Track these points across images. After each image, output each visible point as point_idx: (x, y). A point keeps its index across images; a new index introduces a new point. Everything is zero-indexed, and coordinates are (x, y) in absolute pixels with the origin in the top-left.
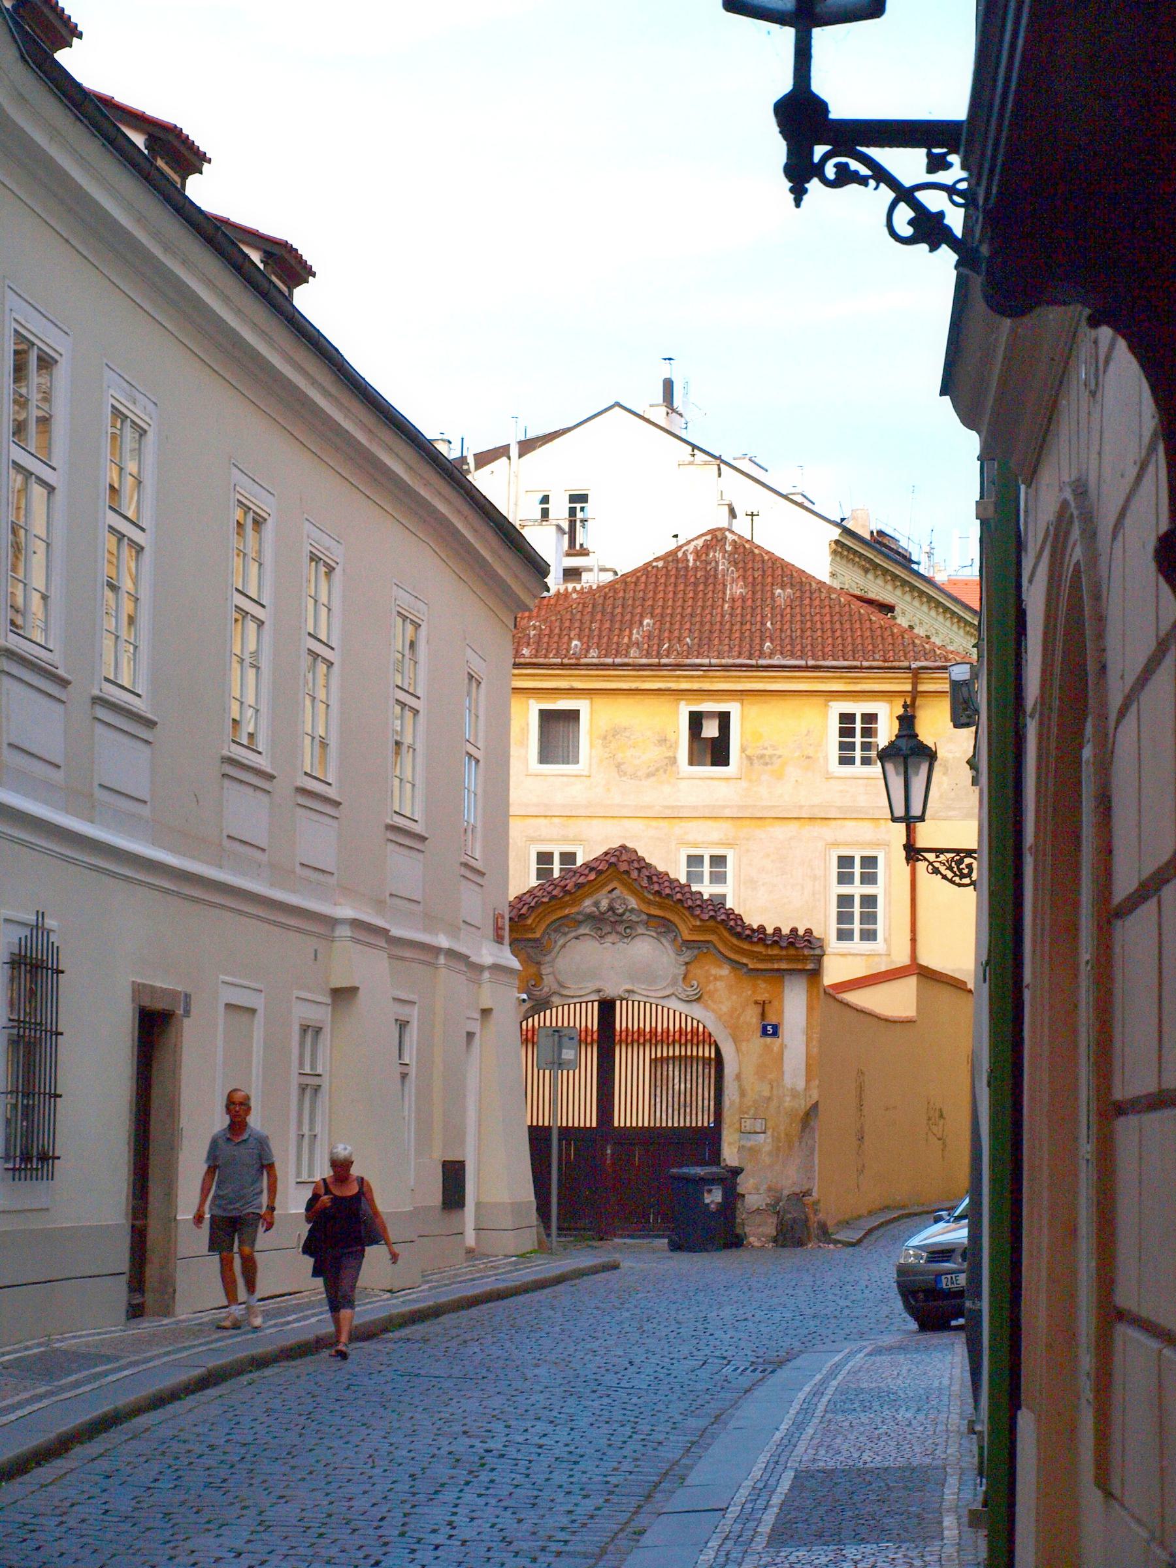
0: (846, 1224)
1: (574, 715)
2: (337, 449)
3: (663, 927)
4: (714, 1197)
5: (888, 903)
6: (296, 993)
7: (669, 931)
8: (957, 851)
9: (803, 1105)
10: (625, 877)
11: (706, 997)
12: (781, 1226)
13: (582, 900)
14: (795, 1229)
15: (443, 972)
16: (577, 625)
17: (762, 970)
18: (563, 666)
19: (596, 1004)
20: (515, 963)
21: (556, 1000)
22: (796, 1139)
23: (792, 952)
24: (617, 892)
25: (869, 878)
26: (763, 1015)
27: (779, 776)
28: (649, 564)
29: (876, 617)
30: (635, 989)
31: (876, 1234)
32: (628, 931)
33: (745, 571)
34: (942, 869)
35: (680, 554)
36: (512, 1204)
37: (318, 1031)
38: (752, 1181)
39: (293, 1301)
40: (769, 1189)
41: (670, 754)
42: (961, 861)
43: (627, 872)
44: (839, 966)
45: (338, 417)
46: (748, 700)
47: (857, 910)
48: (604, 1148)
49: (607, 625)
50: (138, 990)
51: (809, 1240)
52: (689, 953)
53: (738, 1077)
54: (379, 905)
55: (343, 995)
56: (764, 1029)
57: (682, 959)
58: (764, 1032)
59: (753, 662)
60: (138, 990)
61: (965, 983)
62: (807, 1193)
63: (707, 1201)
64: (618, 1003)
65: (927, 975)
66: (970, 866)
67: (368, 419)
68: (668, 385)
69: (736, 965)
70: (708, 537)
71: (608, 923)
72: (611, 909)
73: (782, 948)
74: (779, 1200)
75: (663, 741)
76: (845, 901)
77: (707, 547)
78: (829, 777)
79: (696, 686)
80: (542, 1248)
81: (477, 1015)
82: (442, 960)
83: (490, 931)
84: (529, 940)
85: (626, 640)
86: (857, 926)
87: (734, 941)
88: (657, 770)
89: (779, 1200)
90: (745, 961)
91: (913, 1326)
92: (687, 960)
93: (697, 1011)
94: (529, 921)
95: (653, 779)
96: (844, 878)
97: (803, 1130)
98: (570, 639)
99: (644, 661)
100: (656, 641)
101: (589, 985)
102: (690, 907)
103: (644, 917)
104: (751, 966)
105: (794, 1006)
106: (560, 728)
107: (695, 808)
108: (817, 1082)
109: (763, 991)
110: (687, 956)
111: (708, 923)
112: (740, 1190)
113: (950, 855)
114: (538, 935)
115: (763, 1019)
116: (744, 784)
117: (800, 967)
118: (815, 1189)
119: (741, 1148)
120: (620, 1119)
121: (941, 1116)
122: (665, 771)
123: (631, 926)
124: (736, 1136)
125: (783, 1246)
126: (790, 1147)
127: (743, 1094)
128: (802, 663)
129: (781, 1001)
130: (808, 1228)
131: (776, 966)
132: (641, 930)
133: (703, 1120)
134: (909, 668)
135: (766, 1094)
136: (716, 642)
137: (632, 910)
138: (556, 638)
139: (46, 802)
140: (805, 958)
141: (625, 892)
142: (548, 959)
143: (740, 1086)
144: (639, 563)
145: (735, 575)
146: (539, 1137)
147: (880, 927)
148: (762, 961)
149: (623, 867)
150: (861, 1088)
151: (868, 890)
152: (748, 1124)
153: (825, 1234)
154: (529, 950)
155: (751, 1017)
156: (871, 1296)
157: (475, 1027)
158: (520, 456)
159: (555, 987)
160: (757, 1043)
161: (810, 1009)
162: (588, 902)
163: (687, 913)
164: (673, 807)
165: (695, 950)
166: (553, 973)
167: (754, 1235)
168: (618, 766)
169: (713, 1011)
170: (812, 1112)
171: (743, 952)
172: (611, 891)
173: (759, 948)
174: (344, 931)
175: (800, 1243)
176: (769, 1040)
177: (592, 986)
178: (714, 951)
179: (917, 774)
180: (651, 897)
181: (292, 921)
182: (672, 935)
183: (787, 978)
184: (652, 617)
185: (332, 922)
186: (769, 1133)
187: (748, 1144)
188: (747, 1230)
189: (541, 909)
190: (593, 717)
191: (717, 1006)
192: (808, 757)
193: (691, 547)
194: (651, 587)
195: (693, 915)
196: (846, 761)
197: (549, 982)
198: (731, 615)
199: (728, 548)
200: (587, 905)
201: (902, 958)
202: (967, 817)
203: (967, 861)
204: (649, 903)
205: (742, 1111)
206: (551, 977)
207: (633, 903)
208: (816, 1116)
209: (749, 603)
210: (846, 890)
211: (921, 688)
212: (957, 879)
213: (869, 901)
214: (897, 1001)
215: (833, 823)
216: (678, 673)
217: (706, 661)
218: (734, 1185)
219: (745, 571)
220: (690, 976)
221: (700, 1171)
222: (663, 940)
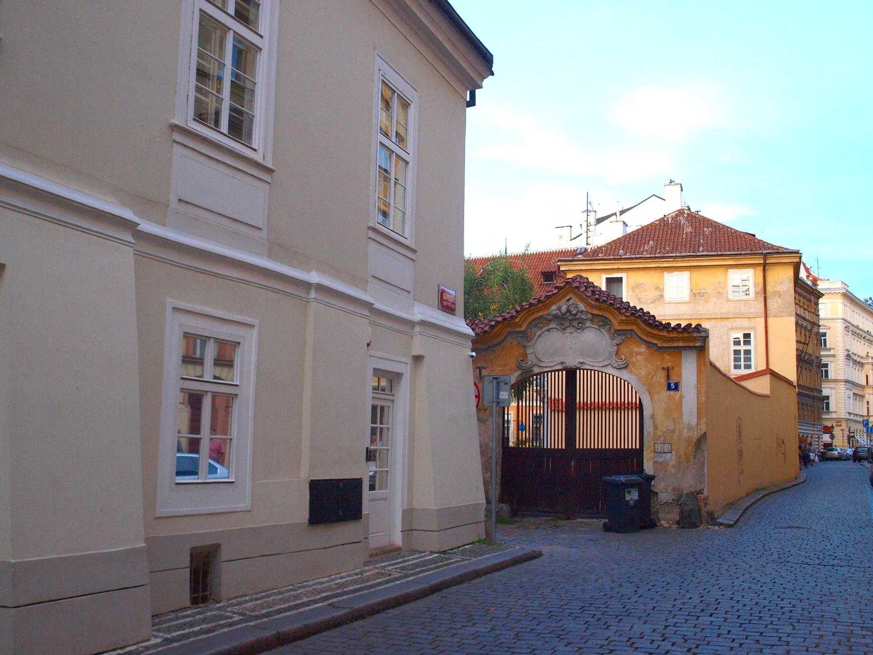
1: (620, 280)
3: (603, 322)
4: (633, 496)
5: (756, 353)
7: (605, 324)
9: (695, 435)
11: (630, 366)
13: (550, 306)
15: (313, 305)
17: (666, 348)
18: (615, 259)
20: (469, 331)
24: (571, 301)
31: (749, 512)
36: (440, 511)
40: (674, 489)
43: (577, 287)
47: (742, 356)
51: (701, 523)
52: (619, 338)
53: (652, 417)
56: (669, 384)
57: (615, 342)
62: (700, 492)
65: (774, 375)
69: (647, 343)
71: (569, 321)
72: (569, 311)
74: (681, 496)
75: (657, 288)
76: (737, 352)
77: (677, 216)
79: (670, 265)
81: (409, 360)
82: (313, 295)
86: (742, 363)
87: (648, 329)
90: (655, 342)
93: (625, 375)
94: (517, 320)
97: (696, 451)
101: (557, 359)
103: (590, 316)
105: (688, 370)
110: (618, 339)
114: (523, 329)
118: (705, 489)
119: (655, 463)
123: (582, 322)
124: (652, 455)
126: (688, 461)
127: (656, 427)
129: (680, 367)
130: (701, 516)
131: (675, 345)
135: (671, 427)
137: (582, 312)
140: (695, 339)
143: (654, 423)
148: (666, 341)
151: (747, 348)
153: (712, 519)
159: (535, 361)
160: (665, 394)
161: (699, 372)
162: (554, 307)
165: (622, 336)
166: (534, 353)
168: (639, 299)
169: (636, 374)
170: (701, 441)
171: (654, 336)
172: (568, 300)
173: (664, 333)
175: (695, 526)
176: (672, 393)
182: (608, 327)
183: (683, 352)
186: (674, 453)
187: (660, 460)
188: (660, 515)
195: (620, 313)
197: (531, 359)
201: (764, 367)
204: (592, 306)
207: (582, 307)
208: (705, 442)
211: (768, 262)
213: (747, 352)
214: (761, 386)
220: (620, 353)
221: (622, 478)
222: (603, 331)
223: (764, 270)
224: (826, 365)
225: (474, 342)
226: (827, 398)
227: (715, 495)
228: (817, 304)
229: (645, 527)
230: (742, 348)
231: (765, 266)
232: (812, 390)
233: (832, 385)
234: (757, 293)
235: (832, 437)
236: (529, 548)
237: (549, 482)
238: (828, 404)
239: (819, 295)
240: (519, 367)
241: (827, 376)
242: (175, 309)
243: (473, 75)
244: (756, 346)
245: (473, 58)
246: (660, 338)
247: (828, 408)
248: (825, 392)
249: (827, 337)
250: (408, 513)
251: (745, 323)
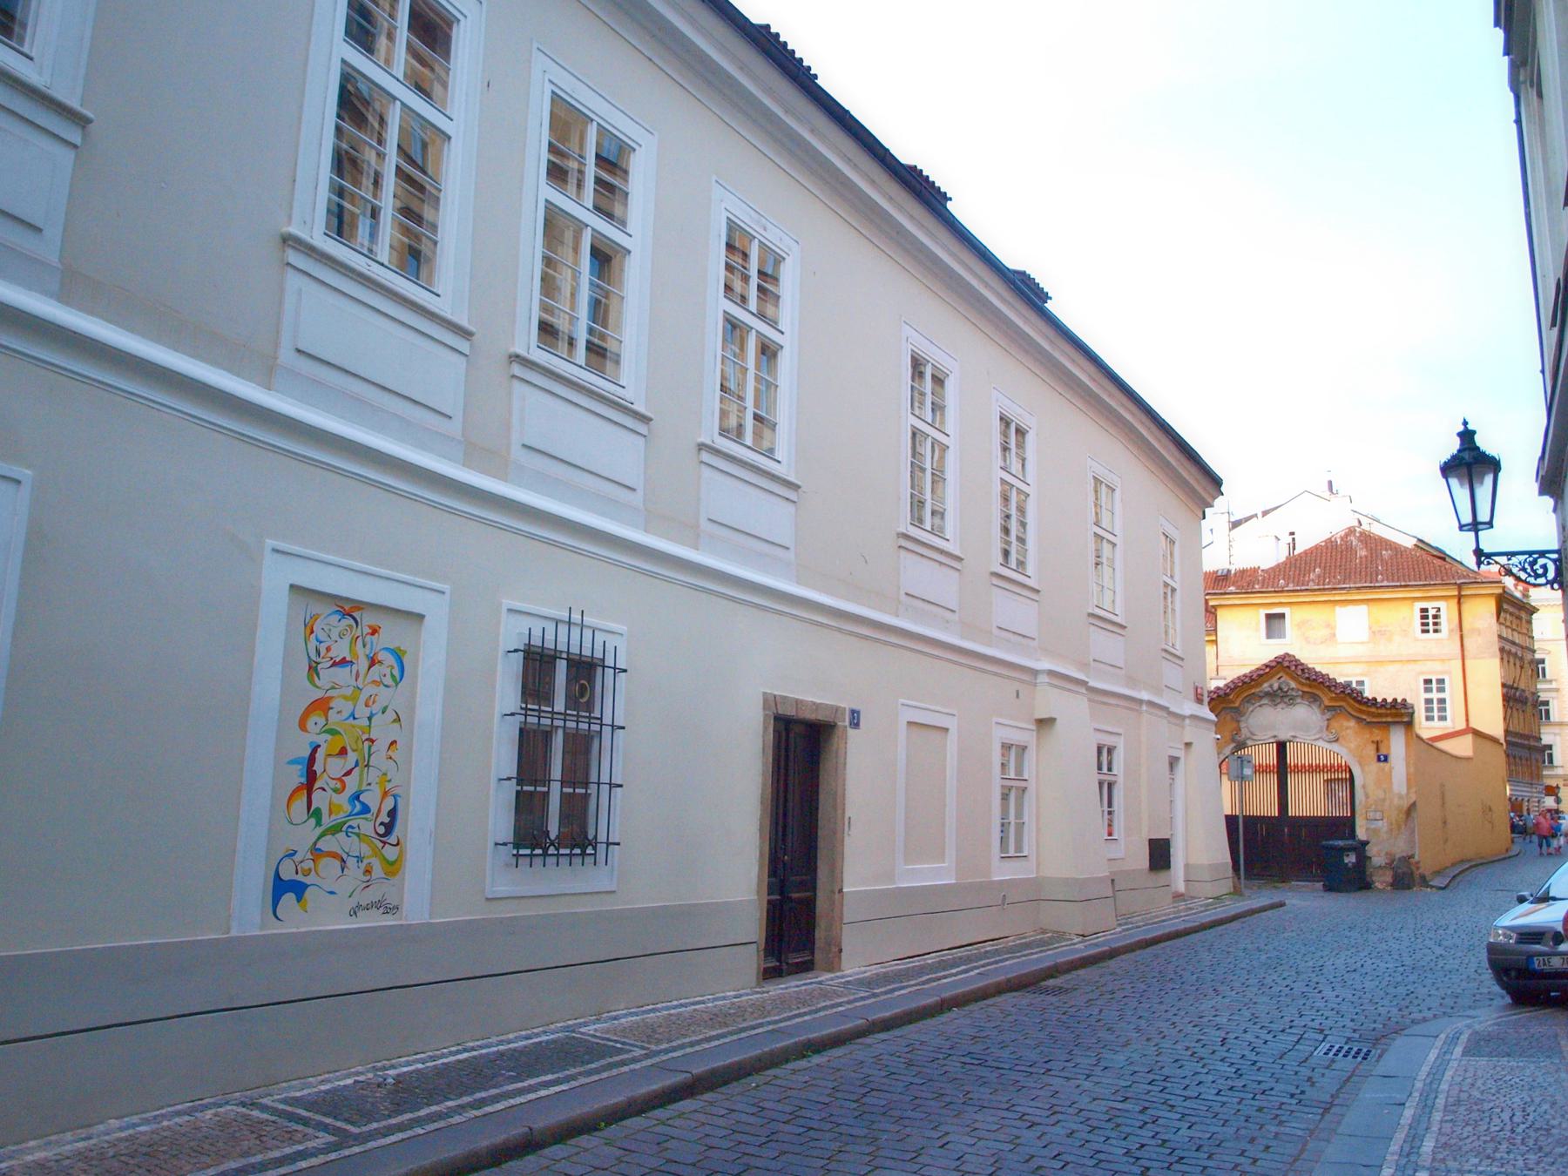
0: (1438, 873)
1: (1282, 616)
2: (1026, 352)
3: (1313, 698)
4: (1351, 859)
6: (995, 719)
8: (1530, 553)
9: (1406, 804)
14: (1405, 878)
20: (1212, 717)
21: (1249, 743)
25: (1441, 690)
29: (1438, 562)
34: (1515, 570)
37: (1024, 748)
39: (1000, 945)
42: (1535, 562)
44: (1426, 728)
45: (1020, 323)
50: (770, 701)
53: (1364, 787)
54: (1083, 666)
55: (1044, 723)
58: (1379, 760)
60: (770, 701)
62: (1412, 856)
65: (1477, 734)
66: (1544, 567)
67: (1050, 332)
68: (1330, 483)
69: (1359, 720)
71: (1279, 697)
75: (1328, 626)
77: (1347, 535)
78: (1416, 640)
80: (1236, 892)
82: (1144, 707)
83: (1192, 696)
91: (1508, 1000)
93: (1335, 747)
96: (1428, 690)
105: (1397, 743)
106: (1276, 622)
109: (1377, 734)
110: (1328, 715)
113: (1522, 558)
123: (1292, 698)
126: (1399, 827)
127: (1367, 796)
139: (443, 456)
146: (1231, 821)
147: (1448, 714)
151: (1441, 695)
153: (1424, 882)
156: (1458, 942)
157: (1180, 753)
160: (1375, 766)
161: (1407, 745)
170: (1410, 810)
174: (1043, 679)
179: (1482, 483)
181: (988, 667)
185: (1035, 673)
190: (1293, 616)
191: (1346, 746)
196: (1424, 631)
197: (1244, 732)
201: (1461, 725)
203: (1541, 561)
207: (1293, 685)
210: (1428, 696)
212: (1532, 580)
213: (1442, 701)
214: (1463, 747)
221: (1341, 843)
223: (1459, 603)
224: (1546, 703)
225: (1216, 724)
226: (1550, 747)
227: (1426, 860)
228: (1530, 622)
229: (1360, 889)
230: (1435, 695)
231: (1460, 598)
232: (1527, 737)
233: (1556, 730)
234: (1451, 631)
235: (1558, 801)
236: (1276, 900)
237: (1276, 849)
238: (1551, 756)
239: (1532, 610)
240: (1233, 740)
241: (1548, 717)
242: (510, 610)
243: (1206, 496)
244: (1453, 694)
245: (1204, 482)
246: (1369, 714)
247: (1551, 761)
248: (1546, 740)
249: (1547, 665)
250: (1187, 866)
251: (1437, 666)
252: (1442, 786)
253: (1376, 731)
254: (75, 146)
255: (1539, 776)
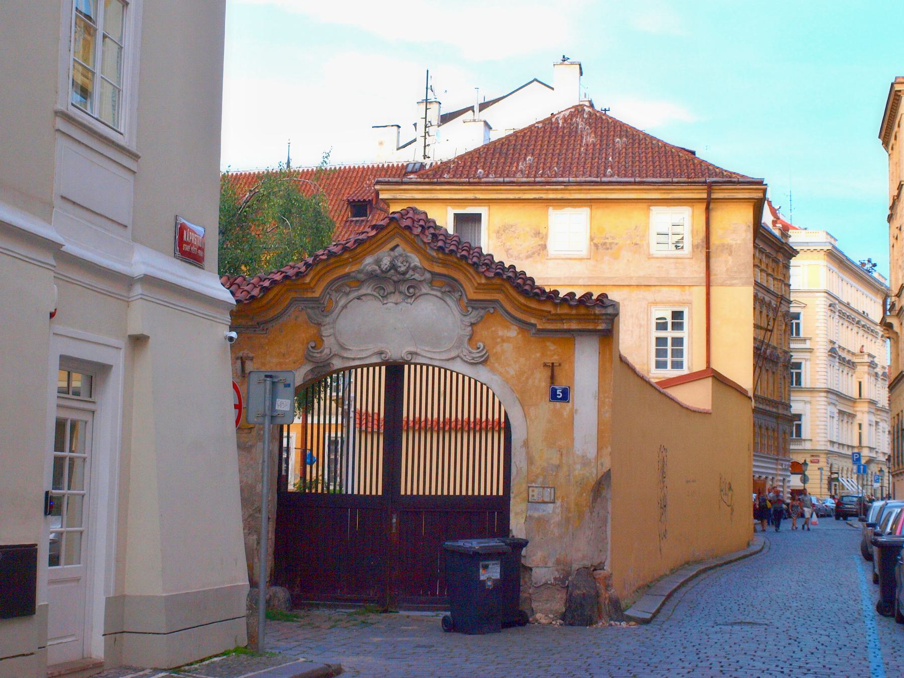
1: (477, 218)
4: (491, 573)
5: (691, 344)
7: (453, 290)
9: (593, 474)
10: (407, 233)
11: (492, 360)
12: (569, 601)
13: (364, 257)
14: (585, 605)
16: (482, 160)
18: (470, 183)
19: (383, 368)
22: (587, 510)
23: (583, 311)
24: (399, 250)
25: (678, 326)
26: (552, 377)
27: (616, 257)
28: (533, 125)
30: (419, 351)
32: (411, 290)
33: (596, 129)
35: (554, 120)
36: (168, 599)
38: (539, 554)
40: (558, 562)
41: (542, 243)
43: (408, 228)
44: (636, 340)
46: (594, 206)
47: (669, 347)
48: (391, 519)
49: (502, 160)
51: (600, 617)
52: (475, 313)
53: (526, 444)
58: (554, 397)
59: (599, 179)
61: (747, 392)
62: (599, 567)
63: (482, 578)
64: (406, 367)
65: (720, 380)
69: (524, 326)
70: (573, 110)
71: (393, 283)
72: (393, 267)
73: (571, 306)
74: (567, 574)
75: (537, 234)
76: (661, 341)
77: (572, 115)
79: (559, 196)
81: (122, 343)
84: (306, 300)
85: (514, 169)
86: (669, 359)
87: (522, 300)
88: (533, 253)
89: (566, 577)
90: (533, 321)
92: (473, 321)
94: (308, 280)
95: (530, 259)
97: (594, 500)
98: (477, 169)
99: (525, 180)
100: (534, 169)
101: (371, 346)
102: (475, 263)
104: (539, 327)
105: (585, 369)
107: (559, 279)
108: (609, 449)
109: (553, 351)
110: (474, 316)
111: (494, 281)
112: (527, 562)
114: (317, 295)
115: (552, 383)
116: (592, 262)
117: (591, 327)
119: (528, 519)
120: (406, 488)
121: (730, 488)
122: (539, 254)
123: (414, 285)
125: (572, 625)
126: (581, 516)
127: (530, 461)
128: (632, 180)
129: (572, 363)
131: (566, 326)
132: (425, 289)
133: (492, 487)
134: (705, 182)
135: (555, 461)
136: (575, 169)
137: (415, 269)
138: (467, 168)
140: (596, 318)
141: (408, 249)
142: (328, 320)
143: (528, 453)
144: (526, 125)
145: (589, 131)
149: (406, 223)
150: (663, 464)
151: (677, 334)
152: (535, 493)
153: (617, 611)
154: (309, 311)
155: (540, 380)
158: (480, 111)
159: (336, 349)
160: (545, 408)
161: (602, 372)
162: (369, 260)
163: (471, 271)
164: (544, 279)
165: (480, 310)
167: (541, 612)
169: (501, 374)
172: (393, 249)
173: (548, 307)
176: (558, 405)
177: (373, 348)
178: (501, 311)
180: (434, 254)
182: (457, 295)
184: (533, 155)
186: (558, 503)
187: (536, 514)
188: (534, 605)
189: (319, 267)
191: (501, 375)
192: (636, 244)
193: (561, 116)
194: (534, 138)
195: (478, 272)
197: (329, 343)
198: (586, 154)
199: (586, 116)
200: (369, 261)
201: (701, 366)
202: (745, 284)
204: (432, 260)
205: (530, 481)
206: (332, 339)
207: (416, 260)
209: (598, 146)
211: (714, 196)
213: (678, 342)
214: (697, 396)
215: (653, 289)
216: (547, 187)
217: (566, 179)
218: (518, 557)
219: (596, 129)
221: (475, 544)
223: (708, 210)
224: (798, 366)
227: (622, 571)
228: (787, 267)
229: (507, 625)
232: (776, 404)
233: (806, 397)
234: (695, 247)
235: (805, 480)
238: (799, 427)
239: (791, 253)
241: (799, 382)
244: (692, 333)
246: (541, 315)
247: (799, 434)
248: (796, 408)
249: (802, 321)
252: (663, 449)
253: (552, 347)
254: (134, 173)
255: (786, 451)
